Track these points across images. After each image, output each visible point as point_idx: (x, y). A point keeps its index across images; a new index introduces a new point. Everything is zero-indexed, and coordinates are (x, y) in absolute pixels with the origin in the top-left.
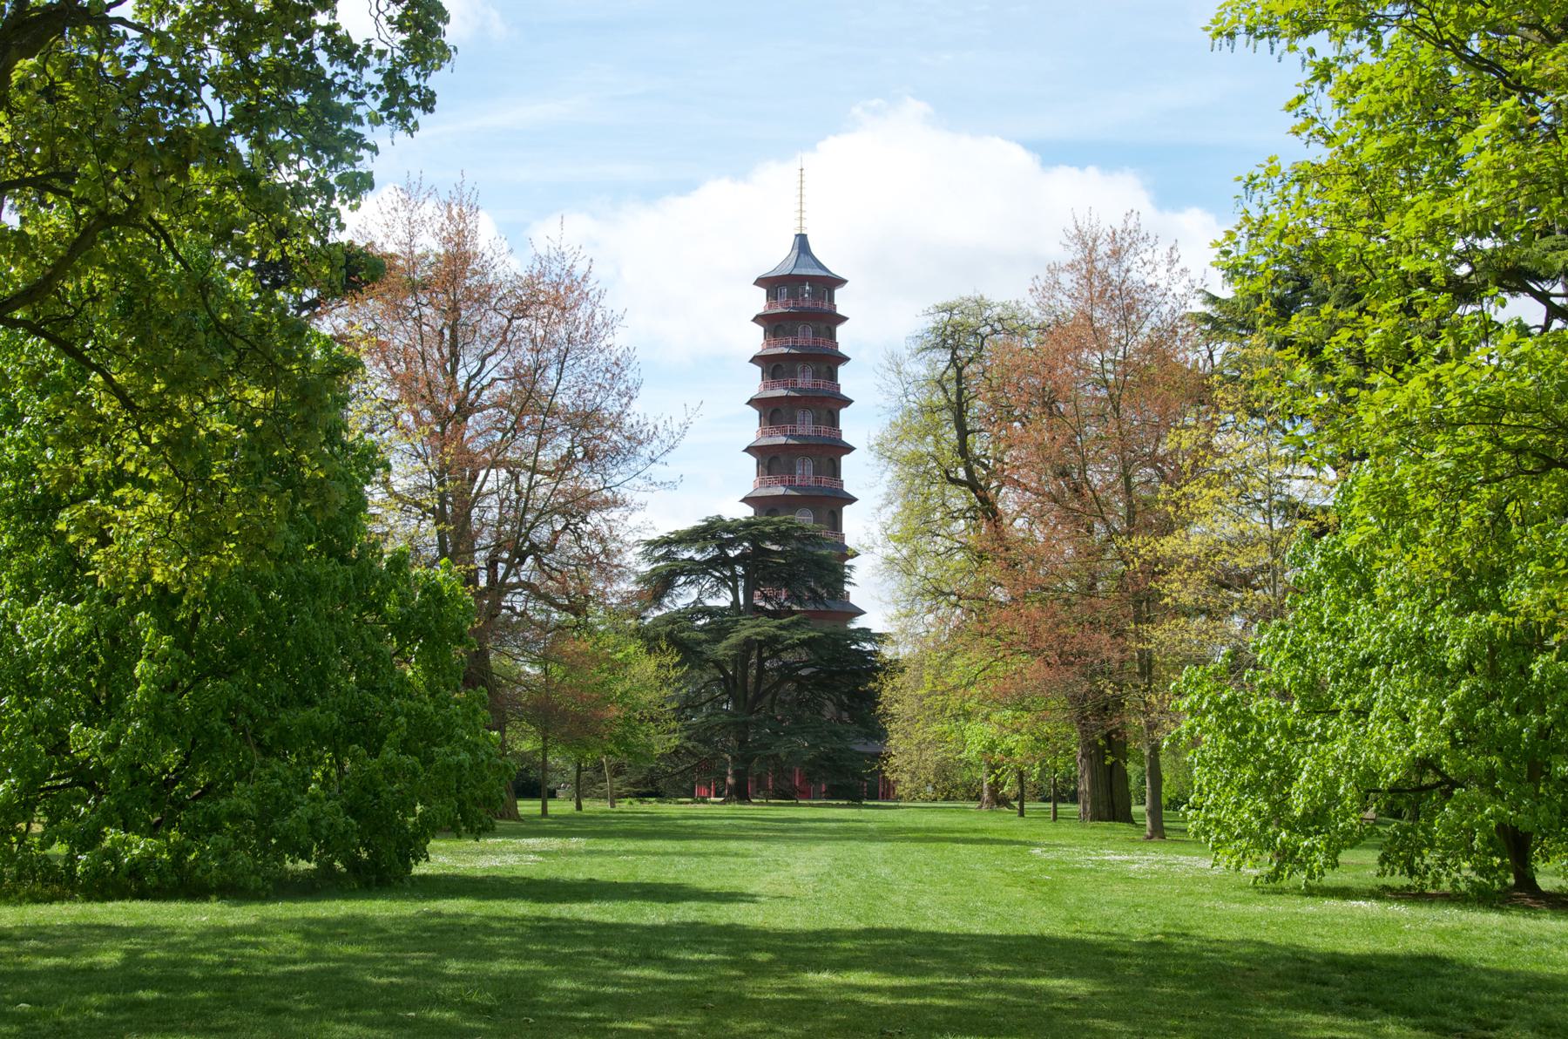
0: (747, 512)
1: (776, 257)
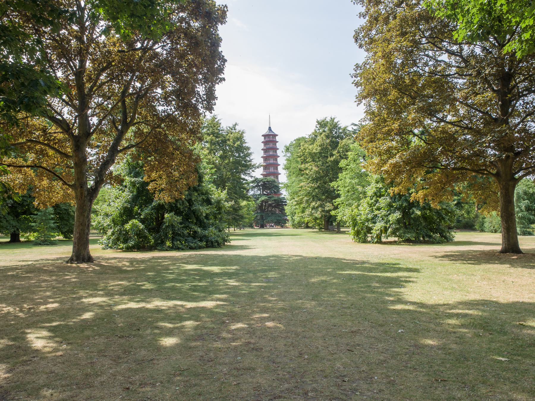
0: (262, 177)
1: (265, 131)
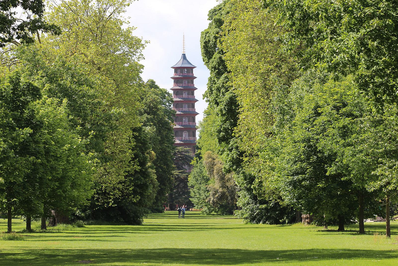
1: (177, 61)
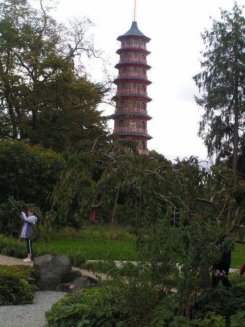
1: (124, 29)
